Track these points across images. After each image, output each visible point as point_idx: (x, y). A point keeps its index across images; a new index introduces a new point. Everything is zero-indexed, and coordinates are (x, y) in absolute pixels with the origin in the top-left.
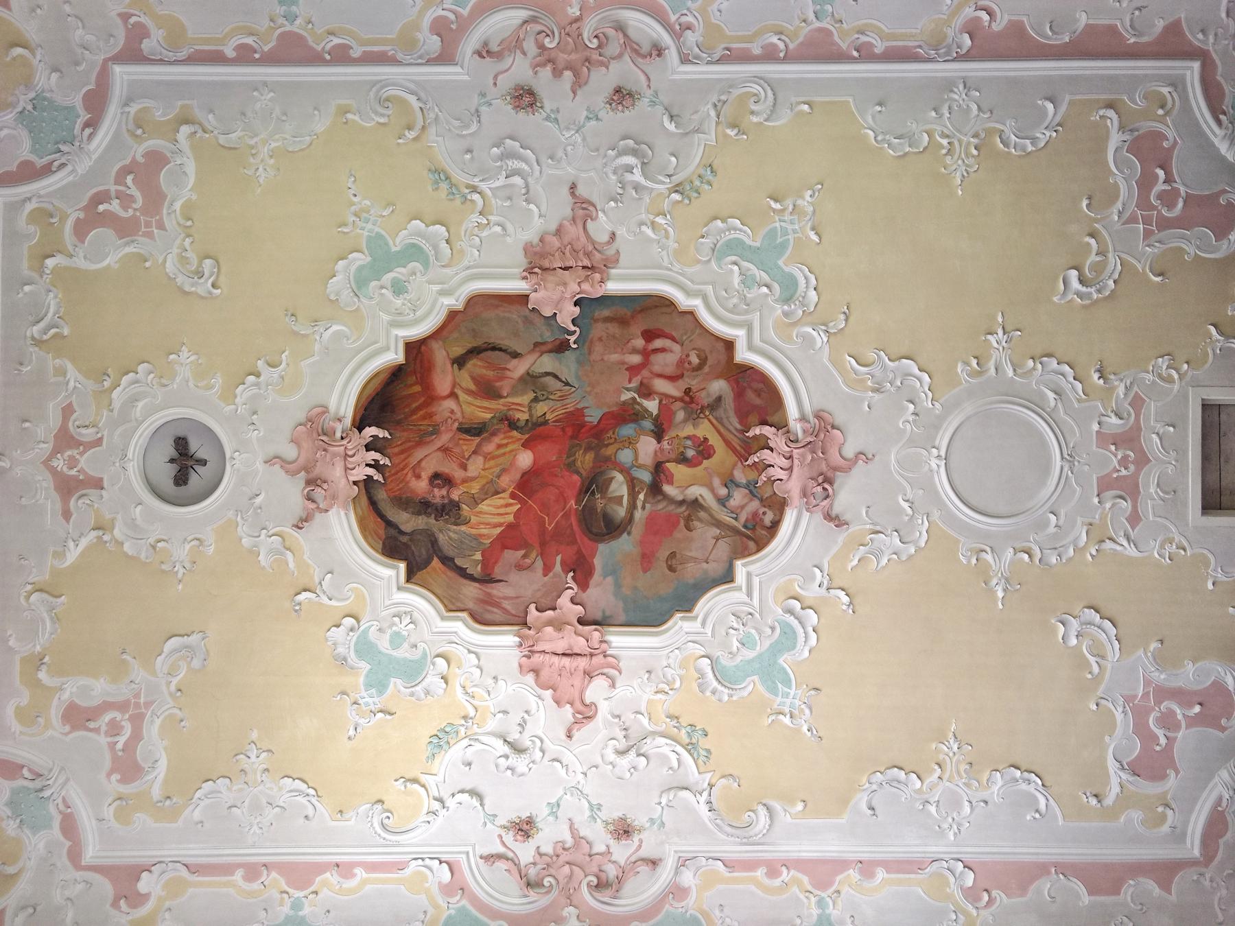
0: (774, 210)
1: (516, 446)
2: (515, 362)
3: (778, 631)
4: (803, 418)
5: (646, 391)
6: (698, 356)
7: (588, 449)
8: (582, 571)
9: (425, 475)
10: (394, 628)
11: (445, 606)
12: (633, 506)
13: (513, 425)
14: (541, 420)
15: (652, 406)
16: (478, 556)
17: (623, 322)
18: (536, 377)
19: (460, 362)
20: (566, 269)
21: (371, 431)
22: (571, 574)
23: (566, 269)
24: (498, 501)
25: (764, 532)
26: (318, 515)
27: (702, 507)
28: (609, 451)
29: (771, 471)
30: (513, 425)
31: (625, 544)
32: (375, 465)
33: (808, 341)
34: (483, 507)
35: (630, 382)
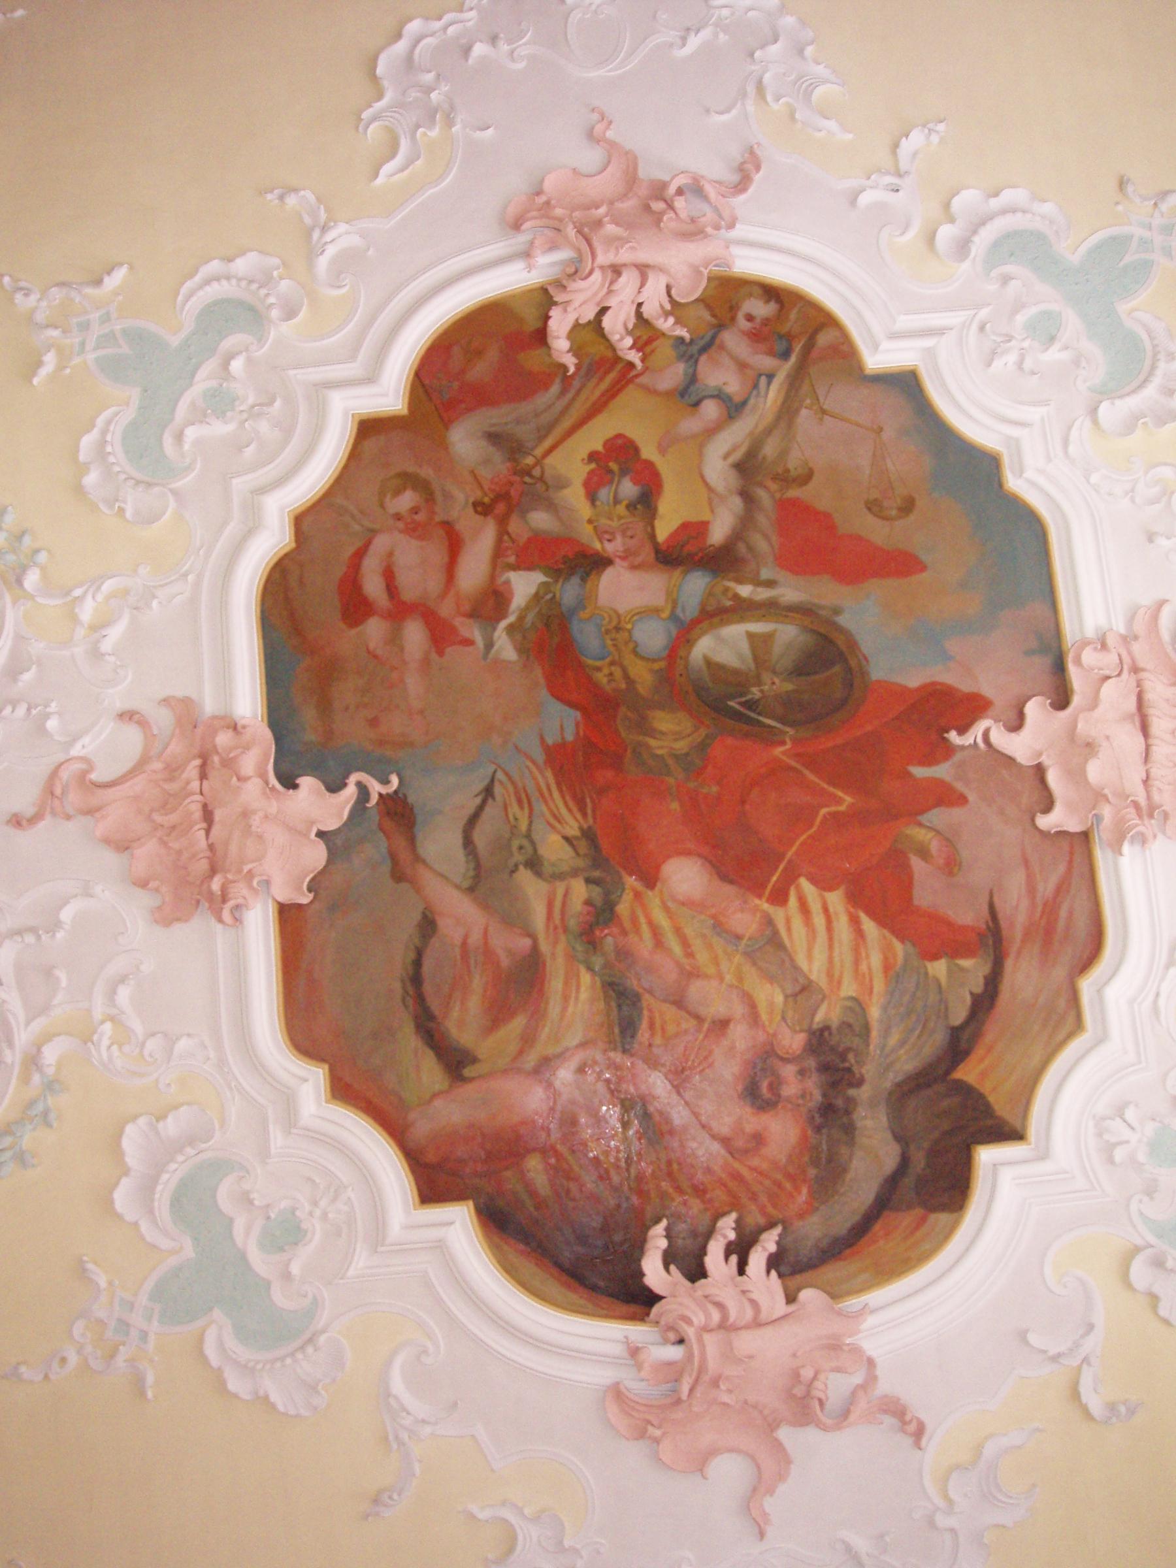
0: (60, 368)
1: (653, 899)
2: (450, 931)
3: (1009, 269)
4: (527, 254)
5: (491, 604)
6: (398, 492)
7: (643, 726)
8: (945, 710)
9: (753, 1122)
10: (1141, 1157)
11: (1070, 1036)
12: (770, 609)
13: (602, 914)
14: (583, 846)
15: (524, 586)
16: (939, 968)
17: (327, 674)
18: (478, 867)
19: (456, 1063)
20: (208, 815)
21: (654, 1271)
22: (953, 736)
23: (208, 815)
24: (796, 935)
25: (793, 315)
26: (886, 1385)
27: (752, 453)
28: (643, 676)
29: (648, 311)
30: (602, 914)
31: (867, 616)
32: (740, 1250)
33: (347, 262)
34: (815, 968)
35: (469, 642)
